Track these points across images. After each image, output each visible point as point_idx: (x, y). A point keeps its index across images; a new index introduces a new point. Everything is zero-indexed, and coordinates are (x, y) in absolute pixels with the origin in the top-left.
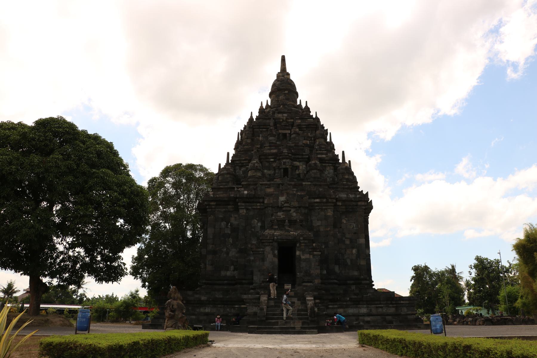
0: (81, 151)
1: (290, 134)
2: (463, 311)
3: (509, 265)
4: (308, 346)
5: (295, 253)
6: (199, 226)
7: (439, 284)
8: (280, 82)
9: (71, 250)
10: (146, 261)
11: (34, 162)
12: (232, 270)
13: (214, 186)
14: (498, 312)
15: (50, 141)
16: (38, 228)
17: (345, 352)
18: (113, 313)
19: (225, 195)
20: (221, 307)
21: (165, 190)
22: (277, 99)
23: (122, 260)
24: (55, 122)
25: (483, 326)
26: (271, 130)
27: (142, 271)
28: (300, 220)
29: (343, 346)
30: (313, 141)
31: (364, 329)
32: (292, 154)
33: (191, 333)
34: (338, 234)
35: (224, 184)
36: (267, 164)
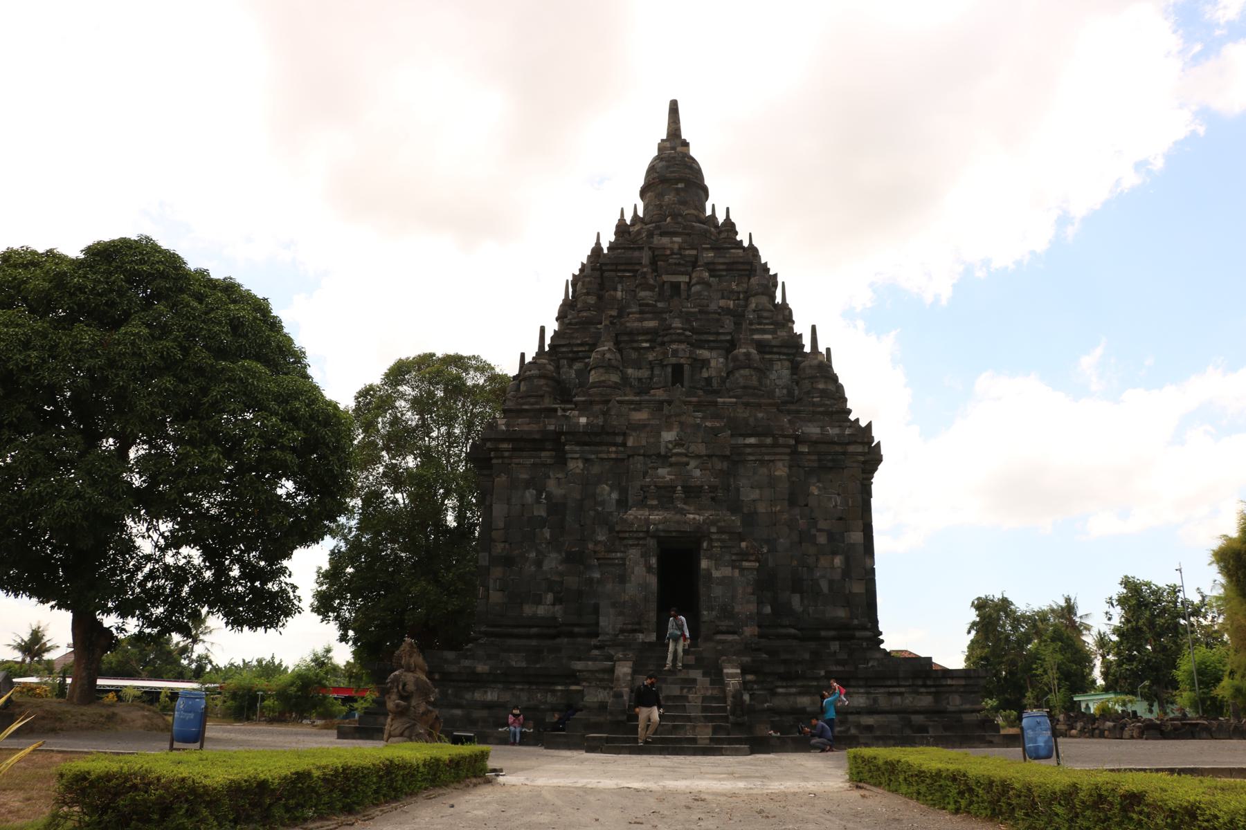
0: (194, 319)
1: (689, 284)
2: (1091, 705)
3: (1200, 598)
4: (728, 785)
9: (170, 553)
10: (350, 581)
11: (81, 343)
12: (548, 603)
13: (510, 405)
15: (121, 293)
16: (90, 499)
17: (817, 801)
18: (272, 701)
19: (534, 427)
20: (522, 690)
23: (290, 576)
25: (1140, 741)
26: (644, 275)
27: (341, 604)
28: (710, 487)
29: (811, 786)
30: (742, 302)
31: (858, 745)
32: (693, 330)
33: (446, 751)
34: (800, 522)
35: (532, 400)
36: (634, 355)
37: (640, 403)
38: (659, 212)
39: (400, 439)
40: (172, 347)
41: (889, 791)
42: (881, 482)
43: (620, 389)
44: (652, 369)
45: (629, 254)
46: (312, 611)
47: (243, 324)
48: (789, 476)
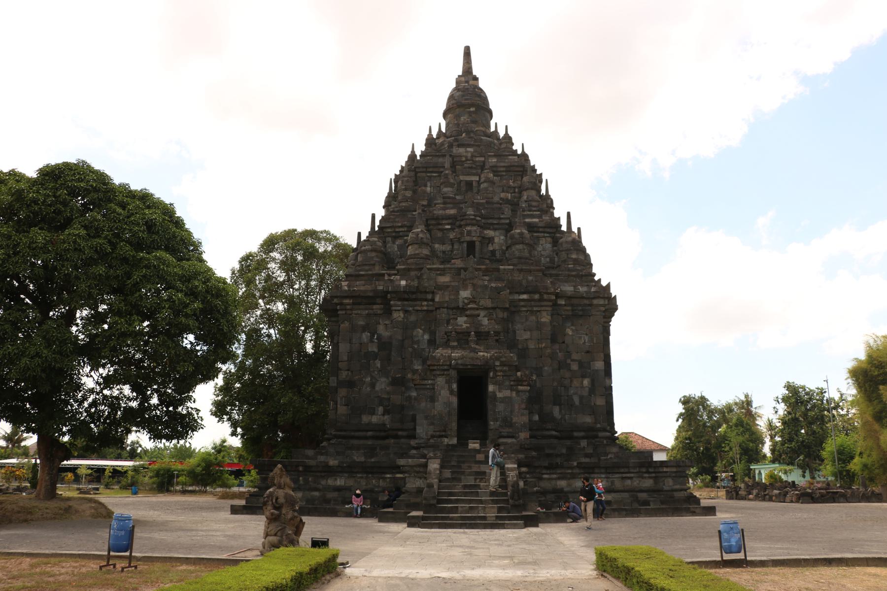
0: (119, 221)
1: (479, 182)
2: (762, 472)
3: (839, 396)
5: (487, 388)
6: (326, 334)
7: (724, 426)
8: (462, 91)
12: (380, 413)
14: (819, 475)
15: (65, 204)
16: (46, 357)
19: (368, 287)
20: (362, 477)
21: (269, 274)
22: (456, 122)
23: (194, 402)
24: (72, 170)
26: (446, 176)
30: (517, 195)
32: (482, 216)
34: (559, 354)
35: (367, 268)
36: (439, 234)
37: (444, 269)
38: (457, 129)
39: (272, 290)
40: (104, 243)
41: (625, 585)
42: (616, 324)
43: (429, 260)
44: (453, 245)
45: (435, 160)
46: (211, 414)
47: (155, 225)
48: (551, 322)
